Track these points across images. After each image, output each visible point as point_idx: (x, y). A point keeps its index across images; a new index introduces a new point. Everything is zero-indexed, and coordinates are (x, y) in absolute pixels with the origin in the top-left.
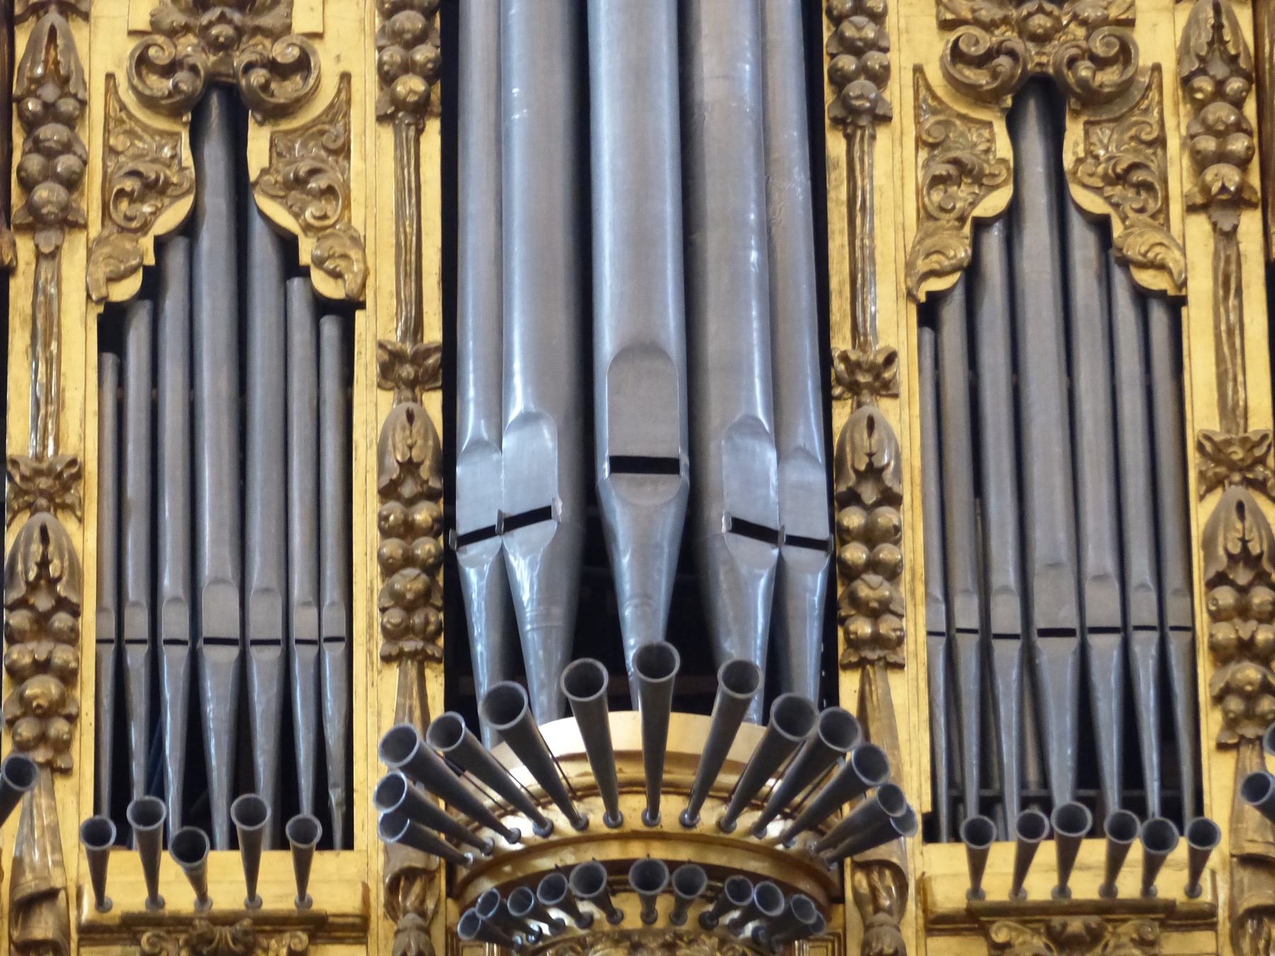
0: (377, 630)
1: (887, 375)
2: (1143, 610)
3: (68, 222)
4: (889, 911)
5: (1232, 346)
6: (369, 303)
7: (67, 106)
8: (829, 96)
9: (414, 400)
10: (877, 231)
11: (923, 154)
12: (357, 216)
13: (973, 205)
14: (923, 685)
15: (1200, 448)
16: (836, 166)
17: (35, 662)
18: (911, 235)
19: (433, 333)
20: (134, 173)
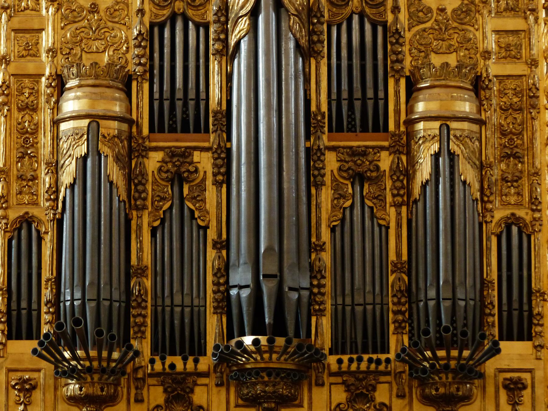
0: (212, 306)
1: (323, 247)
2: (378, 300)
3: (144, 207)
4: (321, 373)
5: (399, 240)
6: (210, 227)
7: (144, 181)
8: (312, 179)
9: (220, 252)
10: (322, 212)
11: (333, 192)
12: (208, 206)
13: (343, 204)
14: (330, 318)
15: (391, 264)
16: (313, 196)
17: (138, 314)
18: (329, 212)
19: (224, 236)
20: (158, 196)
